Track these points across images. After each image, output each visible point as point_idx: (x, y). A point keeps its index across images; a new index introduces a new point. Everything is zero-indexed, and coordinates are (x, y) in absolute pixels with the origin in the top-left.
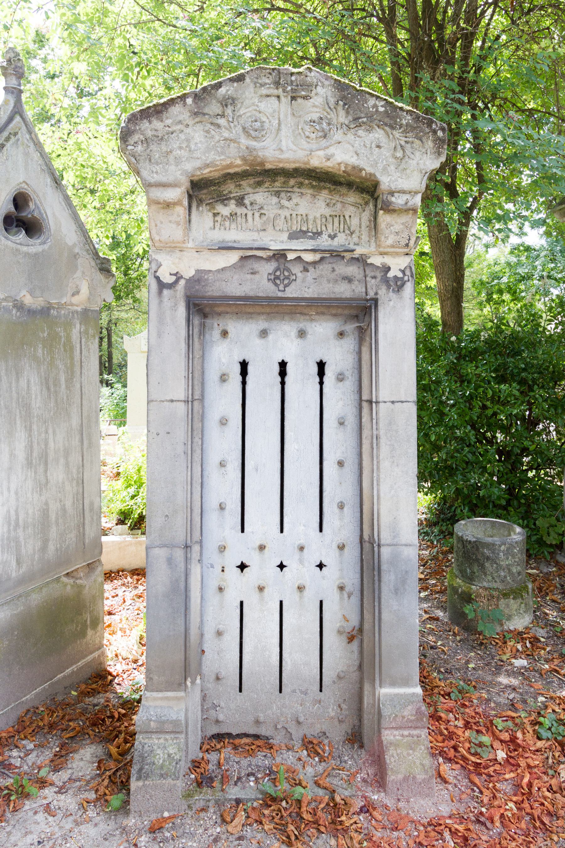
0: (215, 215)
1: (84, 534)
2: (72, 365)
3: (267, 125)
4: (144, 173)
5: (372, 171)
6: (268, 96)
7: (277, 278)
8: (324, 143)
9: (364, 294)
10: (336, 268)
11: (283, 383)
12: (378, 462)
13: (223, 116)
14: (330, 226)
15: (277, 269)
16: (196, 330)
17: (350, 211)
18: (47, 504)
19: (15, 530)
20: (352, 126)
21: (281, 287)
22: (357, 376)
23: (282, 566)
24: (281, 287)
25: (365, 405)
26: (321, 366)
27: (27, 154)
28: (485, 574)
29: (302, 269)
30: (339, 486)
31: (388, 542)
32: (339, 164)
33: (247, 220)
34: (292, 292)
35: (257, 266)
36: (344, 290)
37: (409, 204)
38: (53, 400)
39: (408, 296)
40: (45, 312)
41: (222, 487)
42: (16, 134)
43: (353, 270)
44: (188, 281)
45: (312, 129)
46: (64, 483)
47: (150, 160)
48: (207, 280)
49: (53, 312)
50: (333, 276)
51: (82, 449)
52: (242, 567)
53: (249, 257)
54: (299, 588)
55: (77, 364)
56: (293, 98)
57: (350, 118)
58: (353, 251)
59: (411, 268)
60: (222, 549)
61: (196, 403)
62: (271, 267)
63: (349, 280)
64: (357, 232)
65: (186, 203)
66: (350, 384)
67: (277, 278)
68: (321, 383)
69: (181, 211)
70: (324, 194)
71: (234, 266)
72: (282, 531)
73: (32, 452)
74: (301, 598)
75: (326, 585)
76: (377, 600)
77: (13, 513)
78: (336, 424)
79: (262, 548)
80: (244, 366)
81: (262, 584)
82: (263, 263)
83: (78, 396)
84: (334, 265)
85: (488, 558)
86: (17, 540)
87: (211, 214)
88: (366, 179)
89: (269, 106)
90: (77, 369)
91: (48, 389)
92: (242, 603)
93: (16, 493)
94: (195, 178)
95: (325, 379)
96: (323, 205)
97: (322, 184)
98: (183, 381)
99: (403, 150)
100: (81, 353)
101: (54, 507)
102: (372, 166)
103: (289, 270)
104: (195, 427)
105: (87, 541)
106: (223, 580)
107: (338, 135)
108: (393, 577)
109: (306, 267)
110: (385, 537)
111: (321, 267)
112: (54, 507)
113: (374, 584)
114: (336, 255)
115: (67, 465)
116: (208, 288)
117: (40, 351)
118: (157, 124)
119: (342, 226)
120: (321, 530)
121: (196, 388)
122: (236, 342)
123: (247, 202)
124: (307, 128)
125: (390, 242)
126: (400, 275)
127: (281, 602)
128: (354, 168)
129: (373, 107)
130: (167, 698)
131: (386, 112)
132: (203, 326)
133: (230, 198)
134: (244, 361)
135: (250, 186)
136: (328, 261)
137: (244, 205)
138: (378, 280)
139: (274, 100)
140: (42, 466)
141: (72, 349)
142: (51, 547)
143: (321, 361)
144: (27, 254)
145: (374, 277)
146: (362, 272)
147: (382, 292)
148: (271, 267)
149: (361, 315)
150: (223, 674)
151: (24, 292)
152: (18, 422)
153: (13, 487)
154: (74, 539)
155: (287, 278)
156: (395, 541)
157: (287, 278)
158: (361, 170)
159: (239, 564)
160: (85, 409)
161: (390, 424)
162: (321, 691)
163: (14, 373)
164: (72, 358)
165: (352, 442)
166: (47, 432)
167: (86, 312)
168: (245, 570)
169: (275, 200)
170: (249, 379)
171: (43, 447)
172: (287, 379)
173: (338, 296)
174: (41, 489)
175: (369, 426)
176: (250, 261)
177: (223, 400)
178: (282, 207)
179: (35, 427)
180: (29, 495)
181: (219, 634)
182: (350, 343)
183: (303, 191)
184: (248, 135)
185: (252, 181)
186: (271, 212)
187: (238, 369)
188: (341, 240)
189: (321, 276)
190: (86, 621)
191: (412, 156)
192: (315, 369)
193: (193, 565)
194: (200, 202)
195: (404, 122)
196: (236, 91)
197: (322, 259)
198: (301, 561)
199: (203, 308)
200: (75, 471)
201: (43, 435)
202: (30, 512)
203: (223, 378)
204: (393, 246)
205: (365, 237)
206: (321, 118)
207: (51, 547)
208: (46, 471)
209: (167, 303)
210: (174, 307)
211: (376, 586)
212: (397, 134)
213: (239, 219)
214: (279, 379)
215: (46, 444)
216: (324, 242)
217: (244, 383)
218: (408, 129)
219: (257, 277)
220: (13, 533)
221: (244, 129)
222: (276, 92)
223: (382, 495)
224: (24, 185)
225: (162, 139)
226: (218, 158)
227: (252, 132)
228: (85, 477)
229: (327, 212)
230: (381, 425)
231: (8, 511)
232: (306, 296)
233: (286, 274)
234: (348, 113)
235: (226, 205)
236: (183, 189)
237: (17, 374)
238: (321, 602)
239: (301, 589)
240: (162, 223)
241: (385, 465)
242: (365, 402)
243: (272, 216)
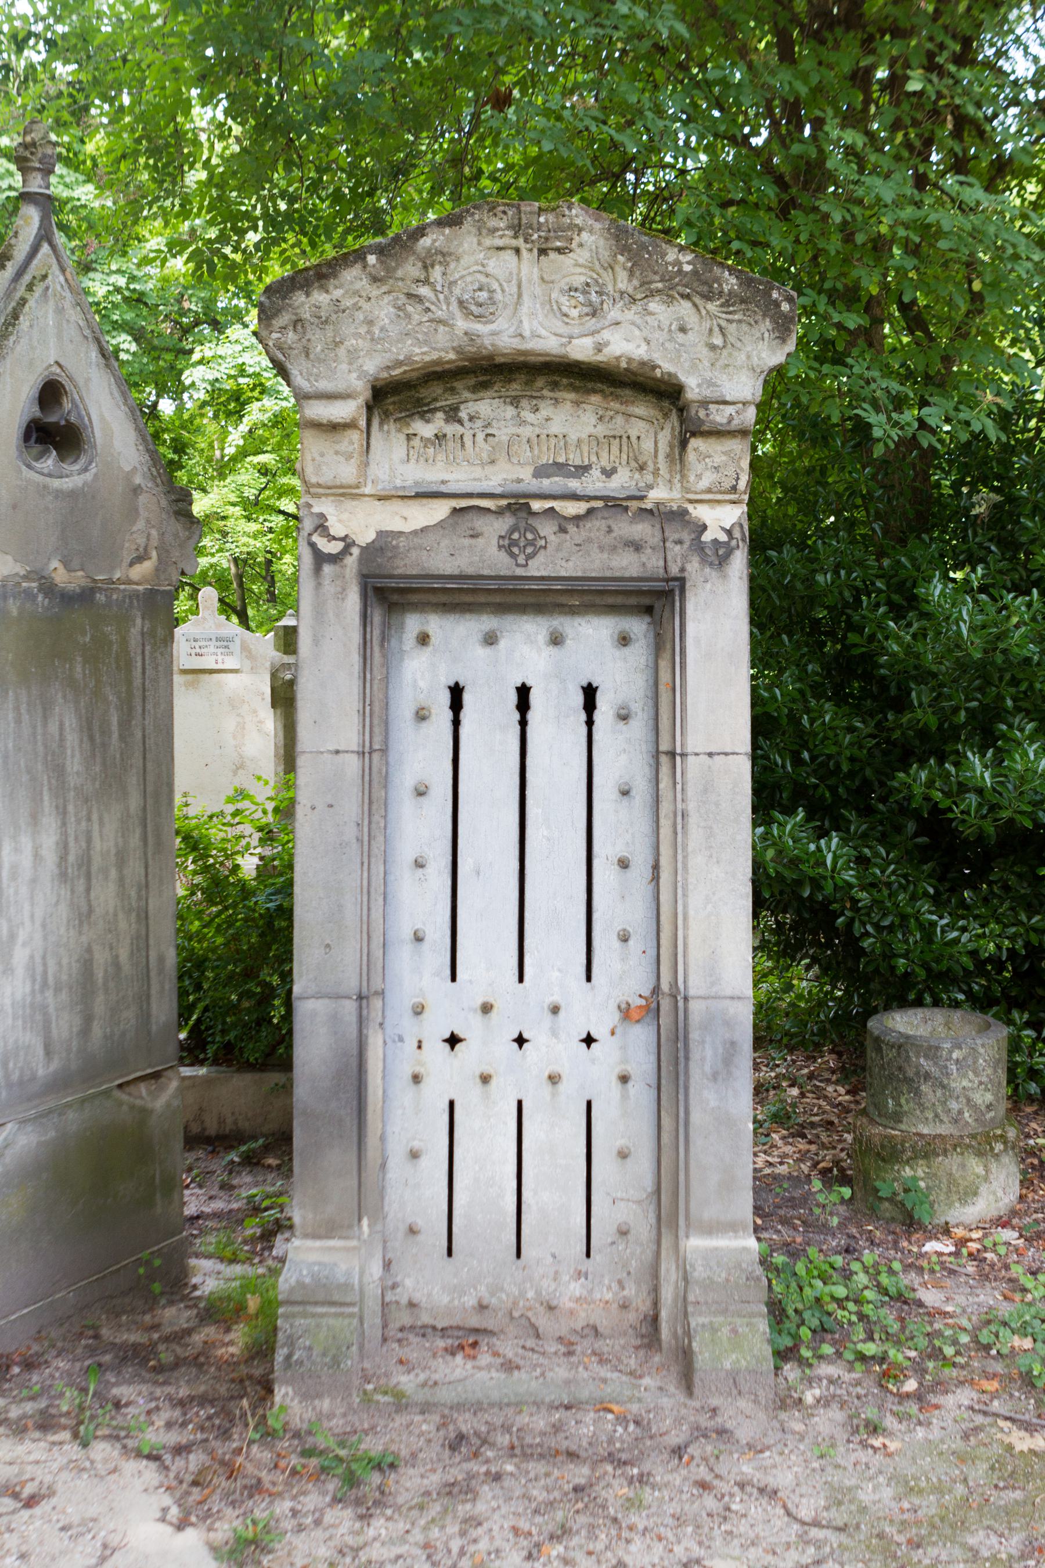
0: (409, 437)
1: (149, 1015)
2: (130, 693)
3: (499, 296)
4: (299, 380)
5: (672, 370)
6: (499, 249)
7: (514, 543)
8: (591, 323)
9: (662, 571)
10: (614, 527)
11: (523, 723)
12: (685, 857)
13: (426, 282)
14: (604, 454)
15: (514, 529)
16: (377, 633)
17: (637, 428)
18: (89, 950)
19: (42, 992)
20: (639, 296)
21: (521, 560)
22: (652, 712)
23: (520, 1041)
24: (521, 560)
25: (664, 760)
26: (590, 693)
27: (60, 311)
28: (923, 1108)
29: (556, 528)
30: (620, 904)
31: (701, 992)
32: (618, 358)
33: (463, 445)
34: (538, 567)
35: (480, 523)
36: (627, 565)
37: (735, 422)
38: (98, 760)
39: (737, 574)
40: (85, 597)
41: (420, 902)
42: (45, 277)
43: (642, 530)
44: (365, 550)
45: (573, 302)
46: (115, 915)
47: (307, 355)
48: (397, 547)
49: (100, 597)
50: (608, 540)
51: (145, 854)
52: (453, 1041)
53: (466, 511)
54: (550, 1077)
55: (138, 693)
56: (543, 252)
57: (636, 282)
58: (641, 498)
59: (741, 526)
60: (418, 1011)
61: (376, 757)
62: (502, 525)
63: (637, 546)
64: (650, 464)
65: (363, 423)
66: (639, 727)
67: (514, 543)
68: (590, 723)
69: (355, 437)
70: (595, 399)
71: (440, 525)
72: (521, 979)
73: (67, 853)
74: (554, 1095)
75: (595, 1073)
76: (681, 1091)
77: (38, 960)
78: (615, 795)
79: (486, 1009)
80: (456, 693)
81: (487, 1069)
82: (491, 518)
83: (138, 754)
84: (610, 522)
85: (927, 1076)
86: (44, 1008)
87: (403, 437)
88: (661, 381)
89: (503, 265)
90: (137, 702)
91: (91, 738)
92: (452, 1104)
93: (44, 926)
94: (379, 384)
95: (597, 716)
96: (593, 420)
97: (590, 385)
98: (355, 719)
99: (724, 335)
100: (144, 673)
101: (101, 957)
102: (671, 360)
103: (534, 530)
104: (374, 796)
105: (154, 1028)
106: (420, 1063)
107: (614, 313)
108: (709, 1053)
109: (563, 524)
110: (696, 985)
111: (589, 525)
112: (101, 957)
113: (677, 1064)
114: (614, 505)
115: (121, 880)
116: (399, 562)
117: (79, 669)
118: (319, 297)
119: (624, 456)
120: (589, 979)
121: (376, 730)
122: (440, 652)
123: (463, 415)
124: (564, 300)
125: (704, 483)
126: (723, 537)
127: (520, 1103)
128: (643, 364)
129: (674, 265)
130: (330, 1249)
131: (695, 272)
132: (386, 626)
133: (436, 410)
134: (457, 684)
135: (468, 388)
136: (600, 515)
137: (460, 422)
138: (686, 546)
139: (509, 256)
140: (82, 881)
141: (129, 665)
142: (97, 1031)
143: (590, 685)
144: (58, 494)
145: (680, 542)
146: (658, 535)
147: (693, 567)
148: (502, 525)
149: (654, 604)
150: (420, 1223)
151: (55, 564)
152: (46, 798)
153: (39, 914)
154: (133, 1022)
155: (531, 543)
156: (713, 991)
157: (531, 543)
158: (654, 367)
159: (447, 1035)
160: (150, 778)
161: (705, 791)
162: (588, 1255)
163: (40, 710)
164: (129, 682)
165: (643, 825)
166: (89, 819)
167: (151, 593)
168: (458, 1047)
169: (510, 411)
170: (465, 716)
171: (84, 845)
172: (531, 716)
173: (618, 574)
174: (81, 923)
175: (670, 795)
176: (470, 516)
177: (421, 754)
178: (523, 423)
179: (71, 808)
180: (62, 930)
181: (414, 1155)
182: (639, 653)
183: (559, 394)
184: (468, 314)
185: (472, 381)
186: (503, 432)
187: (446, 698)
188: (622, 482)
189: (589, 540)
190: (153, 1177)
191: (739, 344)
192: (579, 699)
193: (371, 1032)
194: (386, 415)
195: (726, 288)
196: (448, 240)
197: (590, 511)
198: (554, 1033)
199: (392, 593)
200: (133, 894)
201: (84, 824)
202: (65, 961)
203: (421, 716)
204: (709, 491)
205: (663, 471)
206: (588, 285)
207: (97, 1031)
208: (88, 890)
209: (329, 588)
210: (342, 593)
211: (681, 1067)
212: (713, 307)
213: (451, 444)
214: (517, 716)
215: (89, 841)
216: (594, 483)
217: (456, 723)
218: (730, 301)
219: (480, 541)
220: (39, 998)
221: (461, 303)
222: (514, 243)
223: (691, 913)
224: (57, 370)
225: (326, 322)
226: (417, 350)
227: (473, 308)
228: (151, 907)
229: (601, 430)
230: (690, 792)
231: (32, 957)
232: (563, 574)
233: (530, 536)
234: (631, 273)
235: (428, 421)
236: (361, 401)
237: (45, 710)
238: (589, 1104)
239: (554, 1079)
240: (322, 455)
241: (697, 861)
242: (665, 755)
243: (505, 439)
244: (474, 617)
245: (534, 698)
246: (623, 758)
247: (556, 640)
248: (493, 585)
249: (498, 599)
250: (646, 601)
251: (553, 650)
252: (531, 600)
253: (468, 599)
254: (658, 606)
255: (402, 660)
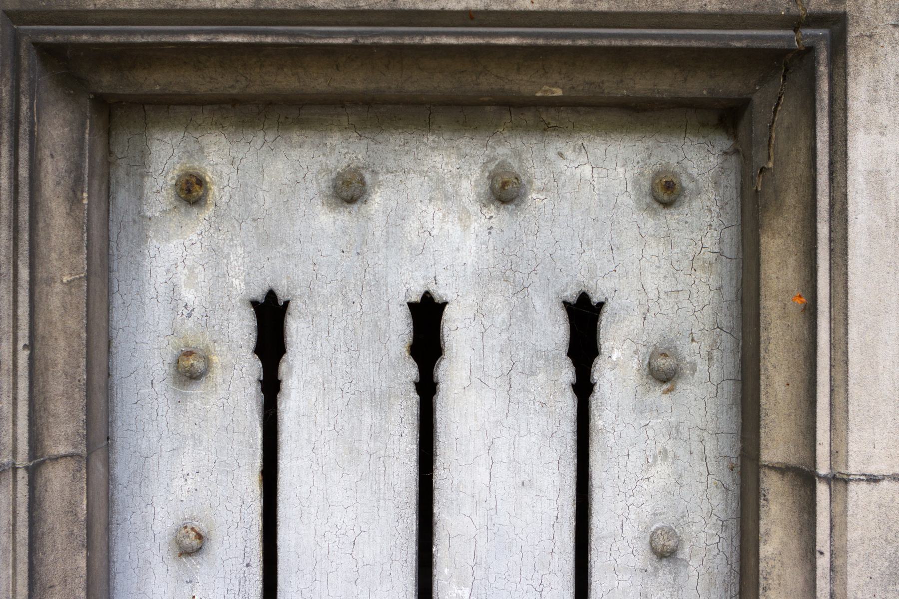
11: (427, 388)
26: (584, 320)
66: (701, 400)
68: (583, 388)
78: (641, 557)
80: (270, 319)
95: (604, 374)
134: (271, 295)
170: (452, 373)
182: (702, 226)
187: (243, 328)
192: (556, 332)
203: (190, 371)
214: (412, 371)
217: (271, 387)
244: (312, 137)
245: (456, 329)
246: (662, 472)
247: (504, 192)
248: (340, 37)
249: (354, 81)
250: (728, 85)
251: (499, 217)
252: (438, 83)
253: (285, 81)
254: (761, 99)
255: (142, 239)
